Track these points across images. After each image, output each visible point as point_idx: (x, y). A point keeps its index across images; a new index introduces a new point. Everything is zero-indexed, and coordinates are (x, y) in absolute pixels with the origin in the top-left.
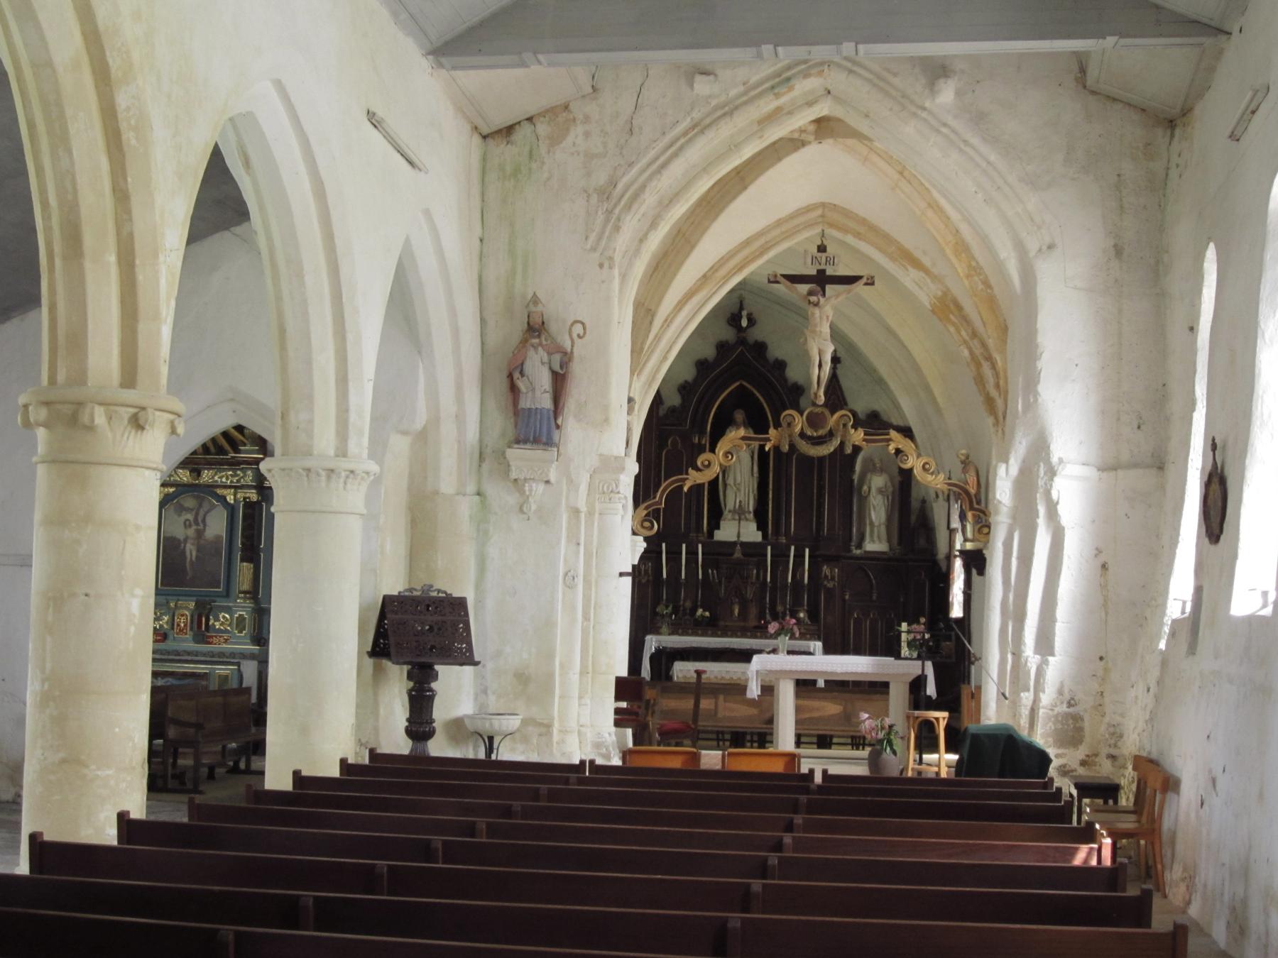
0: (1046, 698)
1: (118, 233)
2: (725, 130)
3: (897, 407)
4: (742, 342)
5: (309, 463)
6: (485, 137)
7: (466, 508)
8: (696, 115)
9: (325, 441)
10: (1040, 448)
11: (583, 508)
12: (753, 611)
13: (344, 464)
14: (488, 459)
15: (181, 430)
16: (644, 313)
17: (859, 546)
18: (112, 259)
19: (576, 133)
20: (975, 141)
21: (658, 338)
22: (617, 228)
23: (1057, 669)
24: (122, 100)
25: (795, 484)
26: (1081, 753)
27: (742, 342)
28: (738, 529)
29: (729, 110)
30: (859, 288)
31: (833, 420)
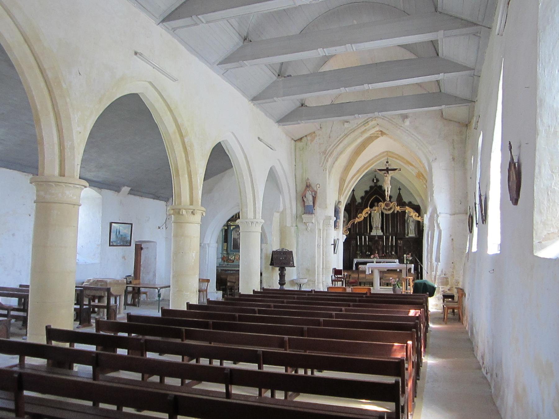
0: (438, 274)
1: (188, 170)
2: (353, 136)
3: (416, 201)
4: (376, 186)
5: (247, 221)
6: (295, 141)
7: (293, 229)
8: (346, 132)
9: (251, 215)
10: (435, 210)
11: (322, 229)
12: (381, 253)
13: (255, 220)
14: (298, 218)
15: (204, 215)
16: (342, 181)
17: (408, 235)
18: (187, 176)
19: (317, 138)
20: (415, 134)
21: (347, 186)
22: (327, 161)
23: (441, 266)
24: (186, 140)
25: (382, 222)
26: (448, 287)
27: (376, 186)
28: (377, 232)
29: (354, 131)
30: (397, 171)
31: (391, 205)
